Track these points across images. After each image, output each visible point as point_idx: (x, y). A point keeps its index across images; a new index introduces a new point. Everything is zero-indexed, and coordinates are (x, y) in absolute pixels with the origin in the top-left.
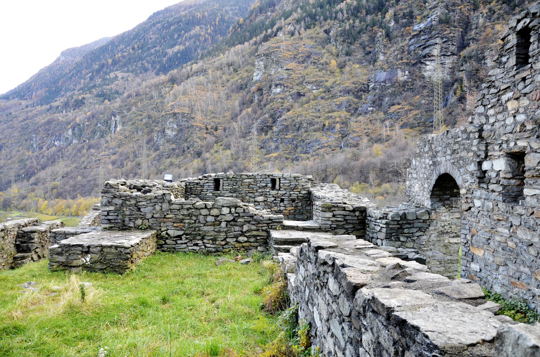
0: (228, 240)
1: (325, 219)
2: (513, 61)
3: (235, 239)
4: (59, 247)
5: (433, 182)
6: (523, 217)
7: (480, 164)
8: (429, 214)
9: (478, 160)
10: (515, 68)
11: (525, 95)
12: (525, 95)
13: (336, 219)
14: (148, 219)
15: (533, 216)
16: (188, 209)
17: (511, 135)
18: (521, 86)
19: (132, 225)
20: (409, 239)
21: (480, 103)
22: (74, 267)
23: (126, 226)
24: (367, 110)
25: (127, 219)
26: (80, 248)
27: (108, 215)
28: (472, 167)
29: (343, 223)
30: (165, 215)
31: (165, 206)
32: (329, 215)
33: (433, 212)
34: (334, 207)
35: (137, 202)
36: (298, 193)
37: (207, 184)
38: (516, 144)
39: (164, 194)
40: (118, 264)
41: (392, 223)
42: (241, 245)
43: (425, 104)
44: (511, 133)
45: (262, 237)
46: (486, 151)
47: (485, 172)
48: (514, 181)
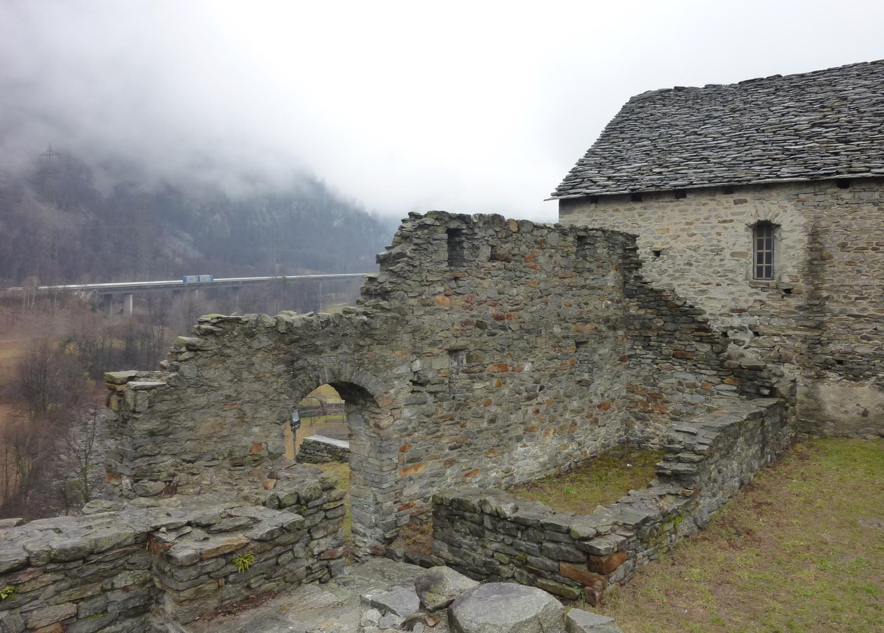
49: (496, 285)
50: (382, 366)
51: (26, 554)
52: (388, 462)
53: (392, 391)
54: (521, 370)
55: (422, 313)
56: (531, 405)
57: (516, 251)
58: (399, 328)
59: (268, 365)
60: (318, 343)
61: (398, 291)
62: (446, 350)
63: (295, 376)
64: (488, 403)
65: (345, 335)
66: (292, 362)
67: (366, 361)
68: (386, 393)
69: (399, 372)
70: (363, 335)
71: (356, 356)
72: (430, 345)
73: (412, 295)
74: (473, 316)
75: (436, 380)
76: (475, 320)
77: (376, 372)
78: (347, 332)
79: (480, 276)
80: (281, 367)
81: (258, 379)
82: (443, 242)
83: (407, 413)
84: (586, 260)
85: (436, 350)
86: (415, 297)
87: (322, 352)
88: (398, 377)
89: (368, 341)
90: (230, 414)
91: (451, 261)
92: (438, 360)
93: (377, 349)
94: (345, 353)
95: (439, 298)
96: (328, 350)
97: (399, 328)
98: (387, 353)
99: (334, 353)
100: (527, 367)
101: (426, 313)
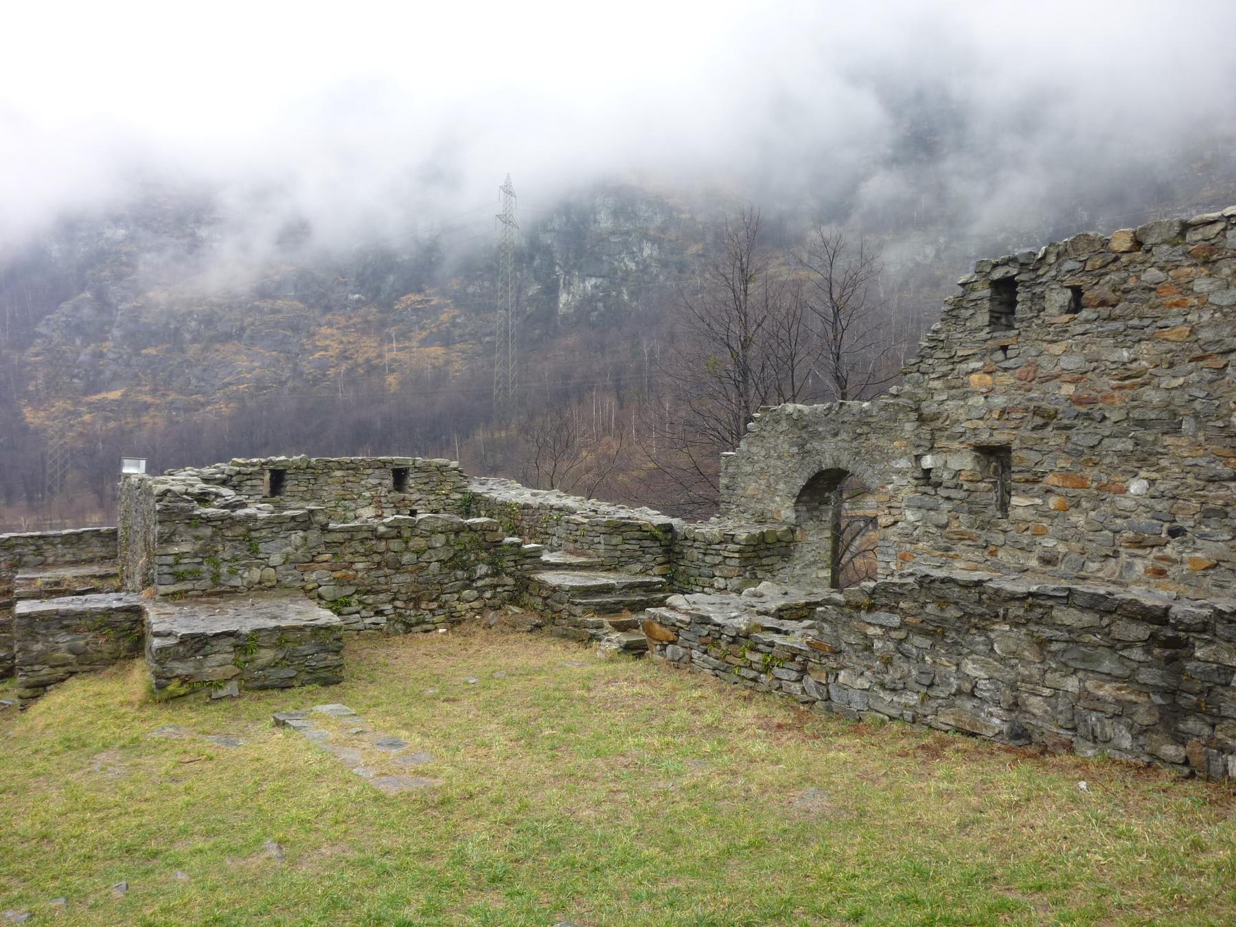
0: (444, 597)
1: (612, 548)
2: (983, 318)
3: (456, 596)
4: (178, 644)
5: (802, 482)
6: (1009, 534)
7: (918, 458)
8: (793, 532)
9: (915, 453)
10: (988, 330)
11: (1006, 369)
12: (1006, 369)
13: (628, 546)
14: (274, 567)
15: (1029, 533)
16: (362, 541)
17: (981, 423)
18: (999, 355)
19: (237, 582)
20: (769, 575)
21: (915, 368)
22: (1064, 641)
23: (224, 585)
24: (347, 298)
25: (224, 569)
26: (232, 640)
27: (177, 563)
28: (903, 464)
29: (638, 553)
30: (314, 556)
31: (313, 535)
32: (616, 540)
33: (798, 528)
34: (625, 524)
35: (250, 530)
36: (444, 497)
37: (249, 483)
38: (991, 435)
39: (311, 511)
40: (322, 664)
41: (748, 549)
42: (467, 606)
43: (474, 295)
44: (981, 419)
45: (506, 588)
46: (933, 439)
47: (929, 470)
48: (984, 485)
49: (1083, 348)
50: (878, 457)
51: (114, 301)
52: (884, 565)
53: (890, 487)
54: (1124, 491)
55: (945, 397)
56: (1143, 557)
57: (1132, 283)
58: (901, 416)
59: (786, 446)
60: (820, 429)
61: (910, 372)
62: (970, 445)
63: (803, 458)
64: (1041, 533)
65: (843, 422)
66: (803, 446)
67: (863, 451)
68: (883, 487)
69: (898, 466)
70: (861, 423)
71: (855, 444)
72: (948, 438)
73: (933, 376)
74: (1031, 400)
75: (950, 484)
76: (1032, 405)
77: (872, 462)
78: (846, 419)
79: (1048, 338)
80: (795, 450)
81: (779, 457)
82: (985, 301)
83: (910, 516)
84: (1215, 262)
85: (956, 445)
86: (939, 378)
87: (824, 438)
88: (898, 472)
89: (865, 429)
90: (762, 482)
91: (994, 322)
92: (955, 457)
93: (873, 437)
94: (844, 440)
95: (974, 377)
96: (829, 437)
97: (901, 416)
98: (883, 442)
99: (835, 440)
100: (1136, 487)
101: (953, 398)
